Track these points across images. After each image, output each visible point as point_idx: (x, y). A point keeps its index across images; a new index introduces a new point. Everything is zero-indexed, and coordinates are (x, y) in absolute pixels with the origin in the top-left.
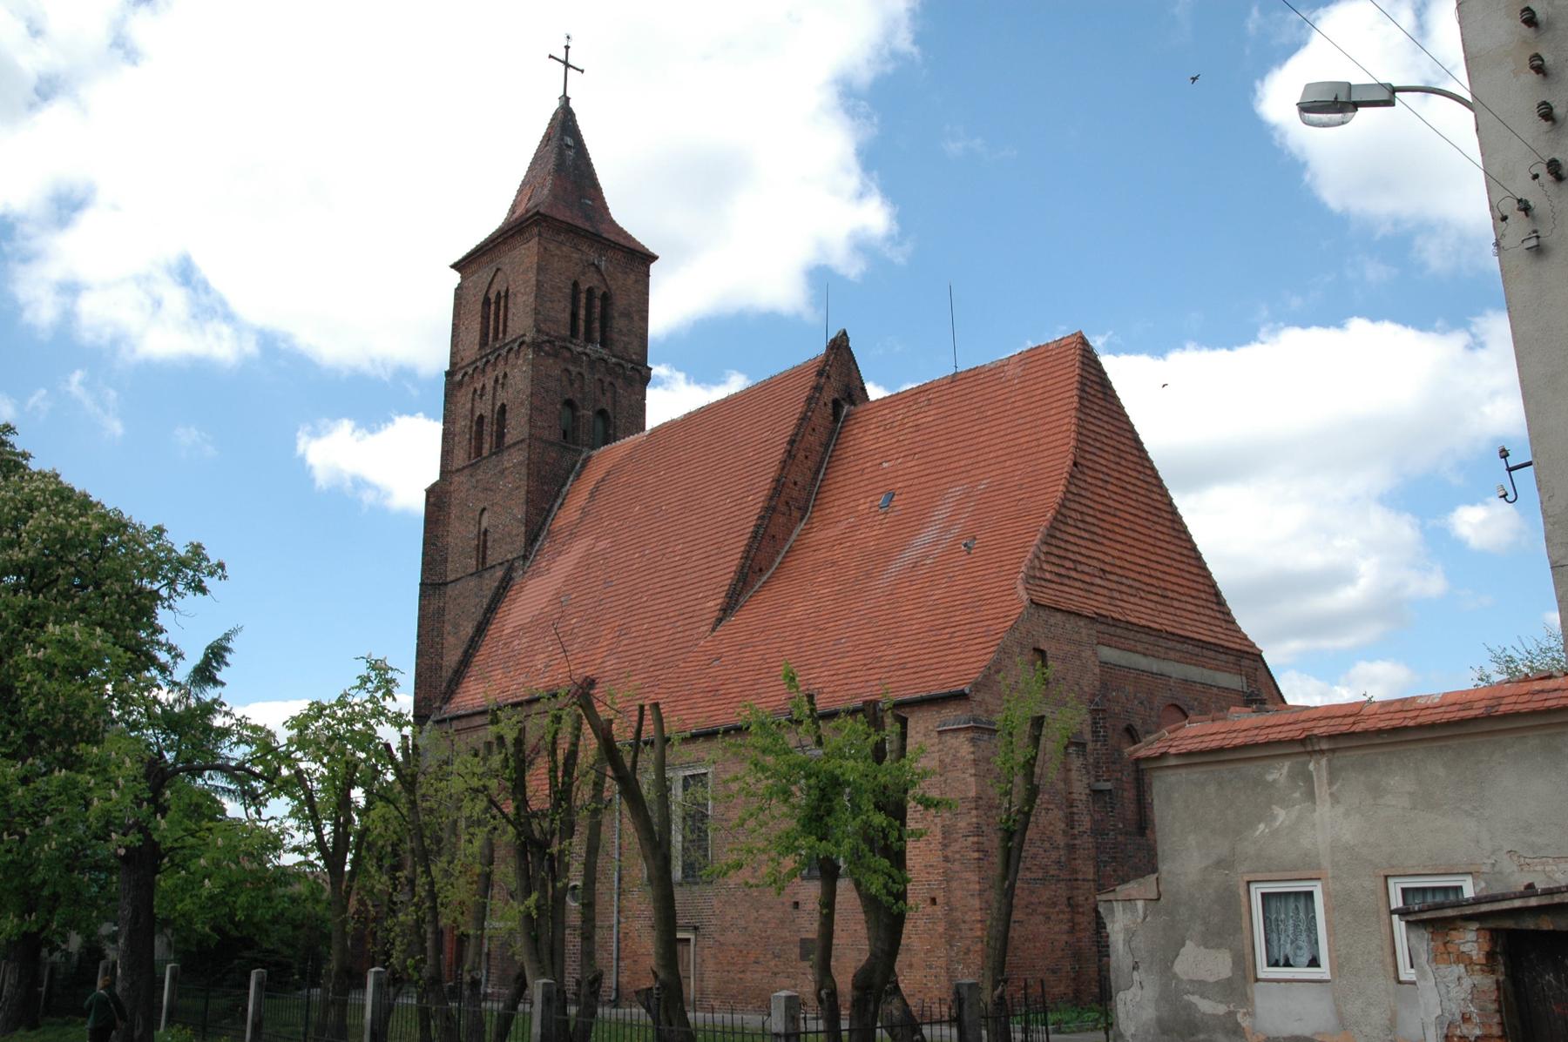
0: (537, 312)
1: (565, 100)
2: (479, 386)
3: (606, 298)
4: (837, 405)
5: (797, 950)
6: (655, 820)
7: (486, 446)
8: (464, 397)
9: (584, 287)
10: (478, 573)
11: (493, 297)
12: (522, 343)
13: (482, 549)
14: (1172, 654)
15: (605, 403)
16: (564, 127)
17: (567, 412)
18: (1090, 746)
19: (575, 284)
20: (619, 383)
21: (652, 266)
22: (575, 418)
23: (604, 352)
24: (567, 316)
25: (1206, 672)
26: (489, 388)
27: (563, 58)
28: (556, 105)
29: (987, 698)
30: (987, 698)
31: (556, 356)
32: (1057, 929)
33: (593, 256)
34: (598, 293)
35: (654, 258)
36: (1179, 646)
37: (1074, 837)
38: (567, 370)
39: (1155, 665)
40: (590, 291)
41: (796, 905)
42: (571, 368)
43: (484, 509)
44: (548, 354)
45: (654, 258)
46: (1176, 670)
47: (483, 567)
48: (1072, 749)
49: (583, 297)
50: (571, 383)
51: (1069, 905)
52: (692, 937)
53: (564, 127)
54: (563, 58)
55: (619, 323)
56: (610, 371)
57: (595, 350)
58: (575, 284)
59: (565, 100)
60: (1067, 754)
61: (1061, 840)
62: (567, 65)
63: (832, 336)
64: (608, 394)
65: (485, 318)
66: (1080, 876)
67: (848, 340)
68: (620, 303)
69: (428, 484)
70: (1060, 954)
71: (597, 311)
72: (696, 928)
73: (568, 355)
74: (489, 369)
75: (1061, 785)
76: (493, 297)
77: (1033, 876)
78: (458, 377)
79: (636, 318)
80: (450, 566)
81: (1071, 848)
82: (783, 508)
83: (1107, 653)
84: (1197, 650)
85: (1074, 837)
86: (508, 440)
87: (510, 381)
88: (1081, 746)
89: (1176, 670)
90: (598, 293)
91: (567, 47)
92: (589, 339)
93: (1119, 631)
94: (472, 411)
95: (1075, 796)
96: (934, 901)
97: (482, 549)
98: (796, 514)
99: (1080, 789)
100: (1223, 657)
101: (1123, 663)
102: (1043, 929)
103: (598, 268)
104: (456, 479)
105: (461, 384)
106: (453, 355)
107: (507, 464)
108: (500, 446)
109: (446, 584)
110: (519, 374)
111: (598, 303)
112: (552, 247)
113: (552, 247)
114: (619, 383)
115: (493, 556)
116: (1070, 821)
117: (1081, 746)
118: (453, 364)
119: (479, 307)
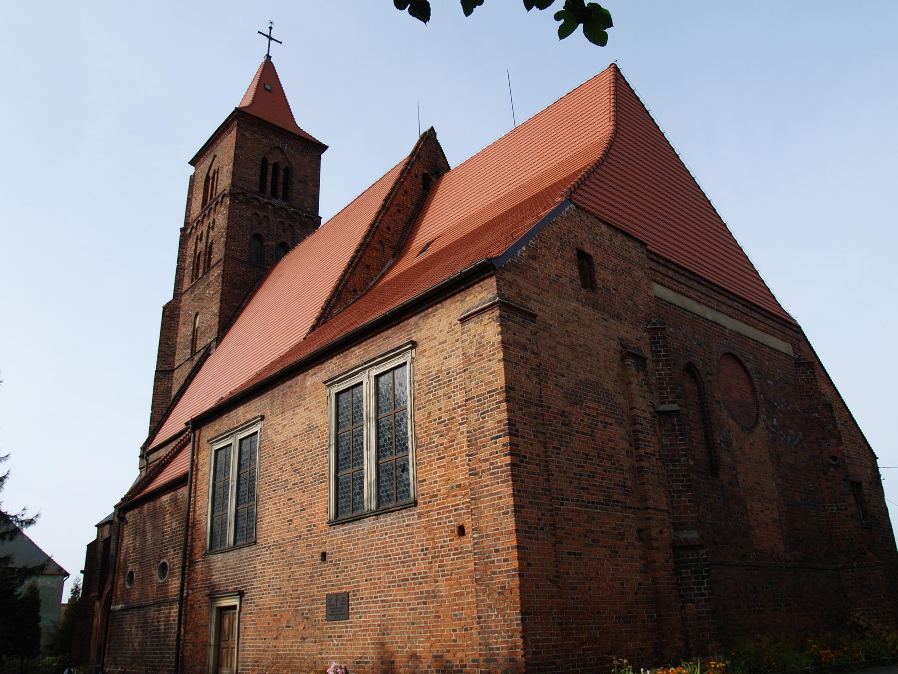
2: (199, 233)
3: (288, 171)
5: (323, 607)
7: (201, 270)
9: (271, 161)
10: (191, 358)
11: (211, 175)
14: (723, 308)
16: (268, 72)
18: (650, 365)
19: (264, 162)
21: (324, 156)
23: (284, 204)
24: (257, 178)
25: (755, 331)
27: (272, 42)
28: (263, 60)
29: (520, 281)
30: (520, 281)
34: (283, 167)
35: (324, 148)
36: (730, 302)
37: (640, 458)
38: (256, 213)
39: (710, 315)
40: (276, 166)
41: (324, 555)
42: (258, 212)
43: (197, 314)
44: (241, 202)
45: (324, 148)
46: (732, 324)
47: (194, 352)
48: (629, 362)
49: (270, 170)
50: (260, 223)
51: (640, 539)
53: (268, 72)
59: (269, 57)
62: (270, 38)
66: (650, 503)
67: (435, 134)
71: (281, 178)
73: (257, 203)
74: (205, 220)
75: (620, 399)
76: (211, 175)
77: (594, 498)
79: (311, 185)
80: (176, 358)
81: (639, 471)
83: (659, 290)
84: (746, 310)
85: (640, 458)
86: (213, 262)
87: (217, 223)
88: (641, 360)
89: (732, 324)
90: (283, 167)
91: (271, 28)
92: (274, 194)
93: (670, 273)
95: (639, 413)
96: (461, 531)
98: (388, 251)
99: (642, 404)
100: (769, 322)
101: (677, 303)
103: (282, 151)
107: (211, 279)
108: (208, 267)
110: (221, 217)
111: (282, 173)
112: (247, 134)
113: (247, 134)
115: (201, 344)
116: (635, 440)
117: (641, 360)
118: (186, 223)
119: (203, 184)
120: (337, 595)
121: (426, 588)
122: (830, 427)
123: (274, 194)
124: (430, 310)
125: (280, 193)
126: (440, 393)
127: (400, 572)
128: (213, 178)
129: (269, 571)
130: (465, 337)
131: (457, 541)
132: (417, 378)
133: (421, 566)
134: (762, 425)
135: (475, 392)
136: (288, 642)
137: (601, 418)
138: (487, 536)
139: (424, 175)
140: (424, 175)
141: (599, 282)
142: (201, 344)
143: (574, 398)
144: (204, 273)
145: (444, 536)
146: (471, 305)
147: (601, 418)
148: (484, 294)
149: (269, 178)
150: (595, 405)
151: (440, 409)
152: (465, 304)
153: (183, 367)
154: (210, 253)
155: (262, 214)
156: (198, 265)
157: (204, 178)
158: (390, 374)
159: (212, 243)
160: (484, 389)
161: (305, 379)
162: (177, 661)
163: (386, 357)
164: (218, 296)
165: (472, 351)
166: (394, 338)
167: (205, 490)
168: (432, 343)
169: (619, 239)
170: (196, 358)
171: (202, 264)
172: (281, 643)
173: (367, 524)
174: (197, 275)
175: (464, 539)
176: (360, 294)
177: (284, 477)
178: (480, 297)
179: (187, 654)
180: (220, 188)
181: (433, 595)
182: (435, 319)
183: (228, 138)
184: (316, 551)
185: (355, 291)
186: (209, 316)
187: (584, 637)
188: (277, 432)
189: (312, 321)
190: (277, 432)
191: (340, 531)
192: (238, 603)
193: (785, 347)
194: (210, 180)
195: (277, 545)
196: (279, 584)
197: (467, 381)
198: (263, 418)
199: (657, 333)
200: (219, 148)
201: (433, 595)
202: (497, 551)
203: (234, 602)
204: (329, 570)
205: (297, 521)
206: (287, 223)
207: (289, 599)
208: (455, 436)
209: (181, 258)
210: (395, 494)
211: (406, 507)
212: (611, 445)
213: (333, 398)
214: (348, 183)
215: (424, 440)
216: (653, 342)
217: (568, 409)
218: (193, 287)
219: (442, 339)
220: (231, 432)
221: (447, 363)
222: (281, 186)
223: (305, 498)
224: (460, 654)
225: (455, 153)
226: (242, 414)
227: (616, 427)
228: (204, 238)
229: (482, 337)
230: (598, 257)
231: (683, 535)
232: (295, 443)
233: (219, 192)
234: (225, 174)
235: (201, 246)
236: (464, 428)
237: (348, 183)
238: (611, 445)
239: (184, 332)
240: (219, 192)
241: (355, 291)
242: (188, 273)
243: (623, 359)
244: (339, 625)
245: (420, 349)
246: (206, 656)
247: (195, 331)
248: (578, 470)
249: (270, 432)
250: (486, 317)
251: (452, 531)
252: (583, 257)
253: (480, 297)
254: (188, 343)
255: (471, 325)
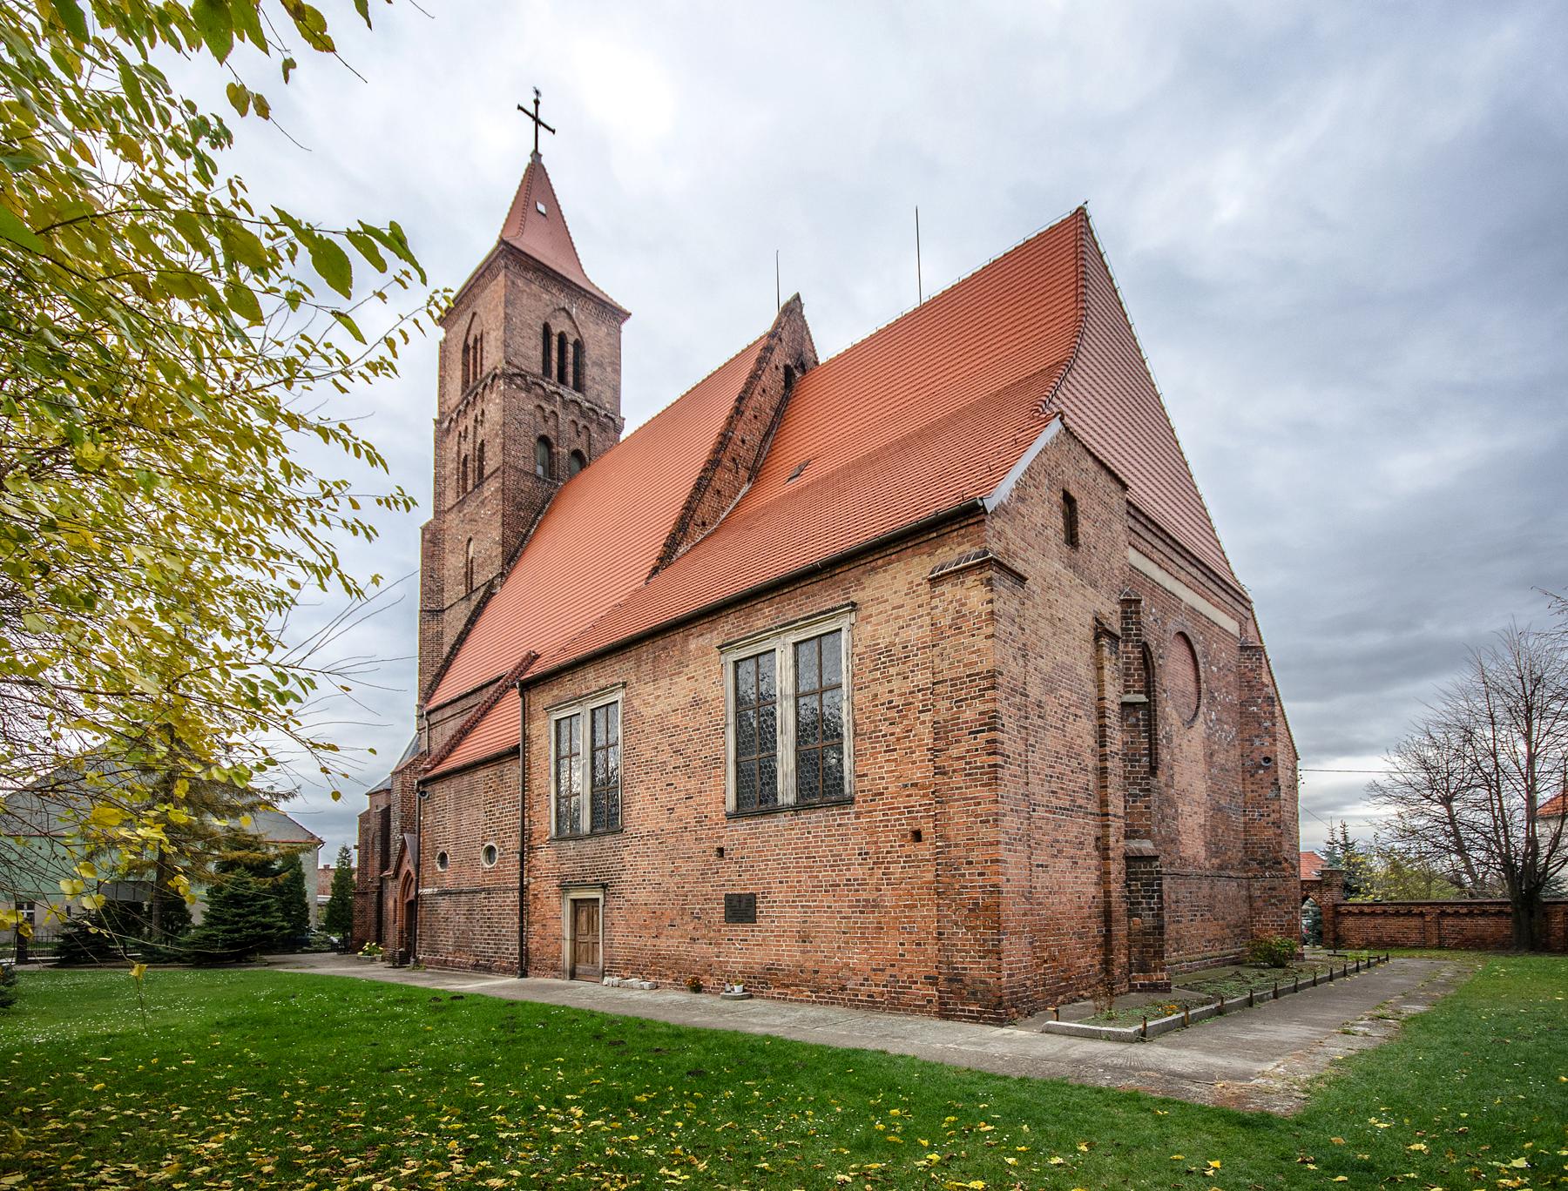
0: (506, 345)
1: (536, 154)
2: (462, 428)
3: (578, 345)
4: (788, 371)
5: (721, 908)
6: (466, 718)
7: (470, 482)
8: (451, 441)
9: (556, 330)
10: (467, 597)
11: (471, 342)
12: (495, 376)
13: (469, 575)
15: (580, 444)
17: (542, 450)
19: (546, 329)
20: (593, 427)
21: (624, 327)
22: (551, 455)
24: (537, 354)
26: (470, 429)
31: (528, 390)
32: (1083, 878)
33: (564, 303)
42: (544, 404)
46: (1189, 597)
47: (471, 591)
52: (598, 895)
54: (541, 128)
55: (591, 371)
56: (583, 414)
57: (568, 393)
58: (546, 329)
59: (536, 154)
60: (1098, 648)
61: (1091, 762)
62: (538, 122)
63: (784, 301)
64: (583, 437)
65: (465, 365)
68: (592, 353)
69: (423, 524)
70: (1086, 912)
72: (604, 886)
73: (540, 392)
76: (471, 342)
77: (1060, 803)
78: (446, 424)
82: (729, 464)
86: (487, 472)
87: (487, 415)
89: (1189, 597)
90: (571, 339)
91: (537, 102)
94: (459, 452)
96: (917, 836)
97: (469, 575)
98: (742, 472)
102: (1069, 877)
104: (448, 517)
105: (448, 430)
106: (441, 404)
108: (481, 479)
109: (443, 611)
111: (570, 349)
112: (520, 283)
113: (520, 283)
114: (593, 427)
115: (479, 579)
118: (441, 413)
120: (740, 895)
121: (864, 895)
122: (1268, 724)
123: (562, 379)
124: (880, 562)
125: (570, 379)
126: (892, 671)
127: (827, 876)
128: (475, 348)
129: (643, 864)
130: (936, 602)
131: (910, 848)
132: (857, 650)
133: (858, 872)
134: (1201, 718)
135: (948, 675)
136: (674, 942)
137: (1072, 710)
138: (956, 845)
139: (787, 367)
140: (787, 367)
141: (1081, 536)
142: (479, 579)
143: (1050, 686)
144: (476, 487)
145: (890, 841)
146: (943, 560)
147: (1072, 710)
148: (966, 547)
149: (555, 355)
150: (1067, 694)
151: (891, 691)
152: (935, 559)
153: (456, 607)
154: (481, 459)
155: (548, 408)
156: (465, 473)
157: (461, 346)
158: (815, 642)
159: (482, 444)
160: (961, 671)
161: (686, 639)
162: (521, 954)
163: (811, 620)
164: (499, 518)
165: (945, 622)
166: (827, 598)
167: (544, 764)
168: (881, 607)
169: (1103, 478)
170: (476, 598)
171: (470, 475)
172: (662, 943)
173: (782, 820)
174: (465, 489)
175: (919, 845)
176: (710, 529)
177: (660, 758)
178: (959, 550)
179: (533, 947)
180: (488, 365)
181: (875, 905)
182: (888, 576)
183: (492, 286)
184: (710, 846)
185: (704, 524)
186: (488, 544)
187: (1046, 955)
188: (646, 704)
189: (652, 562)
190: (646, 704)
191: (742, 828)
192: (601, 897)
193: (1232, 626)
194: (472, 350)
195: (651, 834)
196: (658, 879)
197: (937, 661)
198: (625, 685)
199: (1130, 606)
200: (479, 301)
201: (875, 905)
202: (970, 863)
203: (598, 895)
204: (729, 871)
205: (680, 811)
206: (582, 423)
207: (672, 896)
208: (913, 726)
209: (439, 463)
210: (822, 786)
211: (838, 804)
212: (1079, 741)
213: (731, 667)
214: (662, 366)
215: (867, 727)
216: (1125, 617)
217: (1044, 699)
218: (461, 503)
219: (897, 602)
220: (578, 699)
221: (904, 634)
222: (570, 369)
223: (692, 785)
224: (908, 970)
225: (830, 340)
226: (593, 678)
227: (1084, 720)
228: (470, 436)
229: (964, 605)
230: (1082, 504)
231: (1135, 844)
232: (675, 719)
233: (486, 370)
234: (493, 343)
235: (467, 448)
236: (926, 717)
237: (662, 366)
238: (1079, 741)
239: (454, 564)
240: (486, 370)
241: (704, 524)
242: (452, 483)
243: (1097, 638)
244: (741, 930)
245: (864, 613)
246: (560, 950)
247: (469, 564)
248: (1049, 771)
249: (636, 703)
250: (970, 580)
251: (904, 836)
252: (1069, 500)
253: (959, 550)
254: (461, 577)
255: (946, 588)
